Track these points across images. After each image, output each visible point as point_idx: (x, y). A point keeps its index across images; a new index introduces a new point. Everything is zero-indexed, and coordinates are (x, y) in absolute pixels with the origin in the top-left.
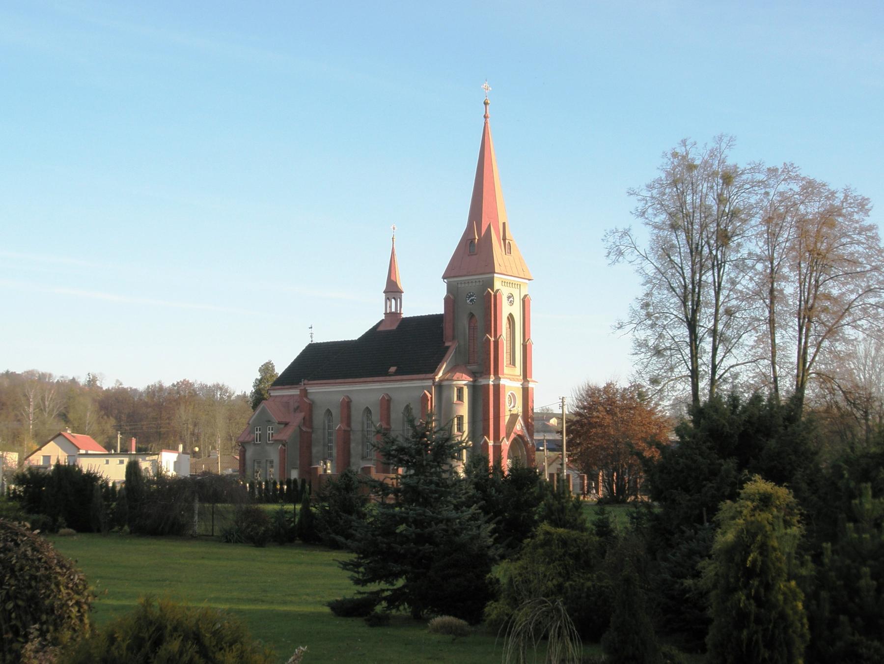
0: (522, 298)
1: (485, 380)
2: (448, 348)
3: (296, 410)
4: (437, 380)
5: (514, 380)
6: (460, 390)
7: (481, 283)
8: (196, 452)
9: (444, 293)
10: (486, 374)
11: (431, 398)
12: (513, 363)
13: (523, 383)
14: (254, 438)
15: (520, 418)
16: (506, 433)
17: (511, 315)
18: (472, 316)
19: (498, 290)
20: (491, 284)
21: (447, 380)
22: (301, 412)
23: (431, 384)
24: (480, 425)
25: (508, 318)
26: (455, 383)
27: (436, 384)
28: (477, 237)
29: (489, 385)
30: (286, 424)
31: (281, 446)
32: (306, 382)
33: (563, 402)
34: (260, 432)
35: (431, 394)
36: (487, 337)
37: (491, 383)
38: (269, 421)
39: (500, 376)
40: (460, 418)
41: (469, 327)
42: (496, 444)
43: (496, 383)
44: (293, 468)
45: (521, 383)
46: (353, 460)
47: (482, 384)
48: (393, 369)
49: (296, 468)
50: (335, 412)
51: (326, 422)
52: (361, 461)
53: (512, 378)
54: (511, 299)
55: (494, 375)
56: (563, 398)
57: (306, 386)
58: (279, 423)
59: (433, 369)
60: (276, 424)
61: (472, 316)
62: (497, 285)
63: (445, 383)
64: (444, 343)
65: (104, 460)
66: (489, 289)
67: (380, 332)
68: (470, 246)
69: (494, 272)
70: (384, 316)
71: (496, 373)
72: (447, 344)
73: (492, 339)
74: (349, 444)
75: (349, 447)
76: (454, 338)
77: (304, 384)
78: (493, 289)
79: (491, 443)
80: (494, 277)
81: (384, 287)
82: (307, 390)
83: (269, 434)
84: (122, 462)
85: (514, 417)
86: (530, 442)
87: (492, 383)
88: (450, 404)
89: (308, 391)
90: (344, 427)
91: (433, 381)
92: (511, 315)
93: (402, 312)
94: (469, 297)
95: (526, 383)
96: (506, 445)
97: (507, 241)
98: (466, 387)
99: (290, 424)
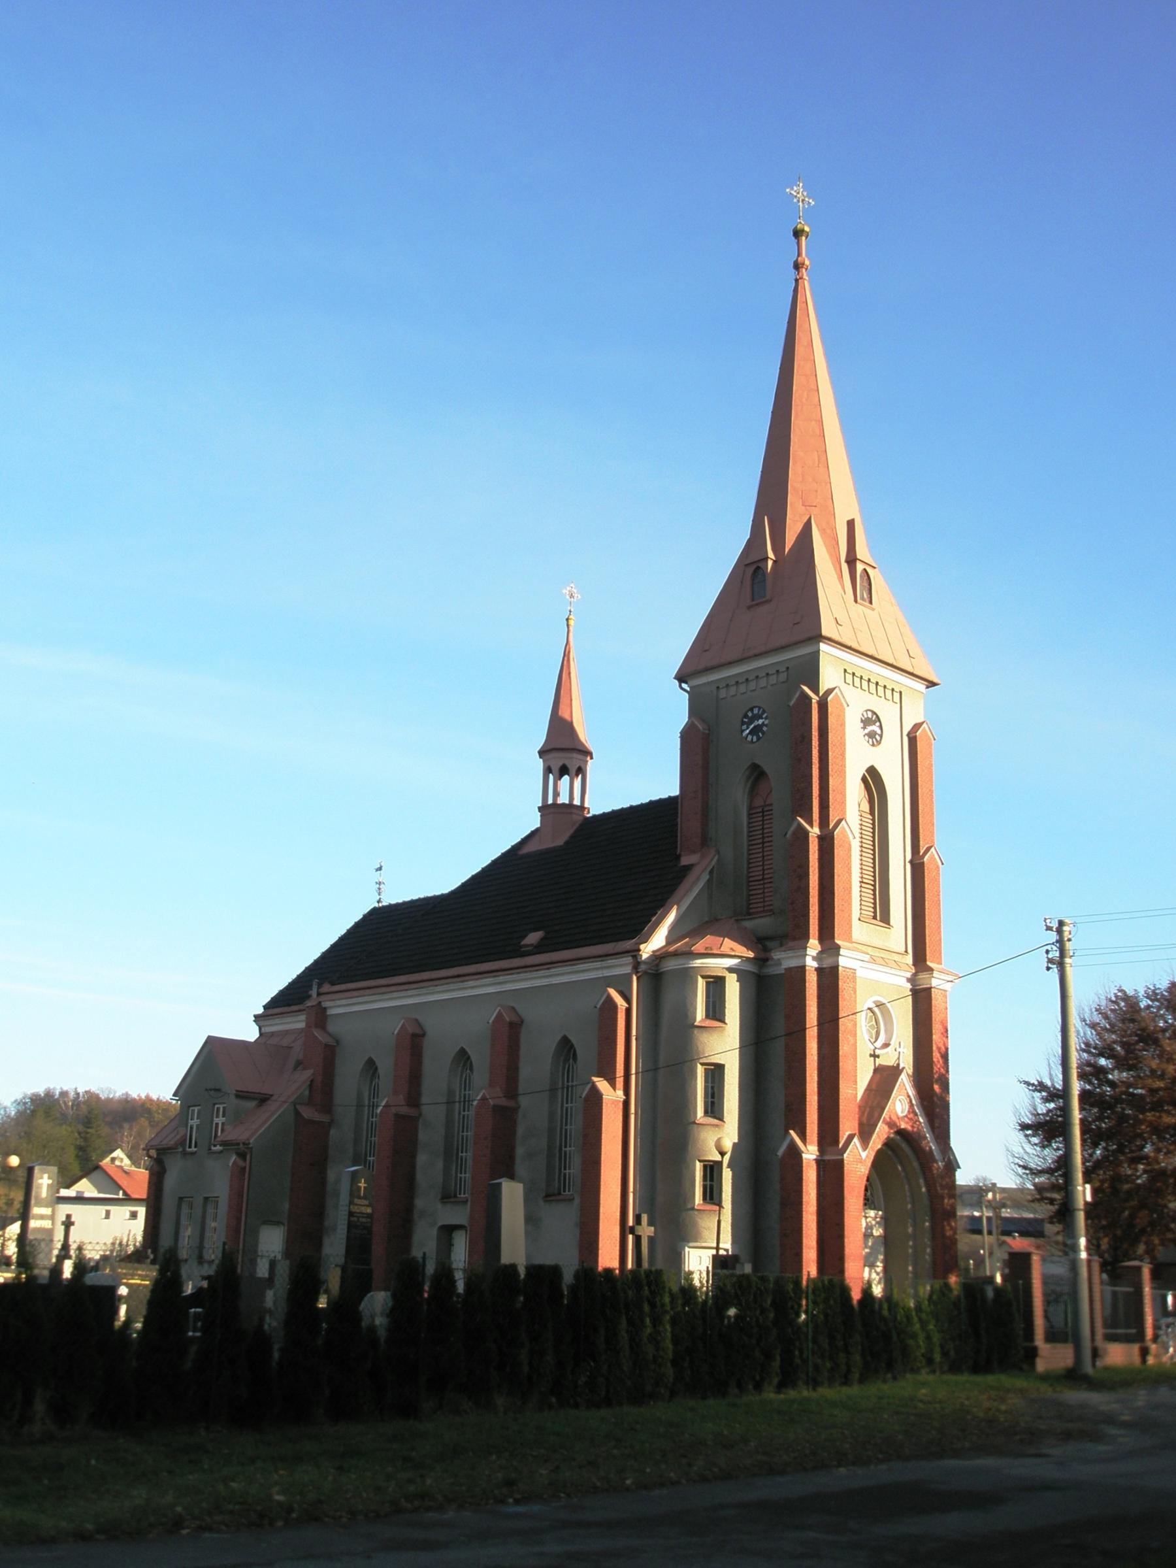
0: (906, 730)
1: (790, 953)
2: (688, 868)
3: (299, 1064)
4: (645, 956)
5: (887, 965)
6: (716, 985)
7: (783, 677)
8: (12, 1168)
9: (682, 717)
10: (794, 939)
11: (628, 1011)
12: (883, 915)
13: (915, 975)
14: (186, 1135)
15: (904, 1078)
16: (861, 1125)
17: (872, 771)
18: (757, 774)
19: (829, 692)
20: (813, 679)
21: (675, 954)
22: (304, 1069)
23: (628, 970)
24: (777, 1096)
25: (864, 779)
26: (698, 963)
27: (643, 967)
28: (771, 555)
29: (803, 968)
30: (263, 1099)
31: (234, 1157)
32: (326, 988)
33: (1061, 943)
34: (374, 1158)
35: (628, 1000)
36: (800, 824)
37: (811, 963)
38: (219, 1090)
39: (837, 942)
40: (716, 1073)
41: (750, 808)
42: (827, 1158)
43: (828, 963)
44: (266, 1222)
45: (909, 975)
46: (419, 1203)
47: (780, 970)
48: (533, 938)
49: (278, 1223)
50: (386, 1066)
51: (366, 1094)
52: (439, 1206)
53: (880, 957)
54: (875, 728)
55: (821, 940)
56: (1061, 923)
57: (322, 998)
58: (241, 1095)
59: (640, 928)
60: (232, 1097)
61: (757, 774)
62: (829, 676)
63: (671, 965)
64: (678, 857)
65: (101, 1209)
66: (806, 689)
67: (528, 855)
68: (753, 584)
69: (819, 637)
70: (537, 817)
71: (827, 933)
72: (685, 861)
73: (815, 831)
74: (413, 1156)
75: (413, 1166)
76: (705, 841)
77: (319, 994)
78: (816, 690)
79: (810, 1153)
80: (818, 651)
81: (540, 740)
82: (325, 1009)
83: (217, 1124)
84: (134, 1215)
85: (885, 1078)
86: (937, 1154)
87: (815, 964)
88: (686, 1029)
89: (330, 1012)
90: (497, 1098)
91: (635, 957)
92: (872, 771)
93: (586, 805)
94: (752, 720)
95: (922, 976)
96: (860, 1161)
97: (860, 567)
98: (734, 976)
99: (273, 1098)
